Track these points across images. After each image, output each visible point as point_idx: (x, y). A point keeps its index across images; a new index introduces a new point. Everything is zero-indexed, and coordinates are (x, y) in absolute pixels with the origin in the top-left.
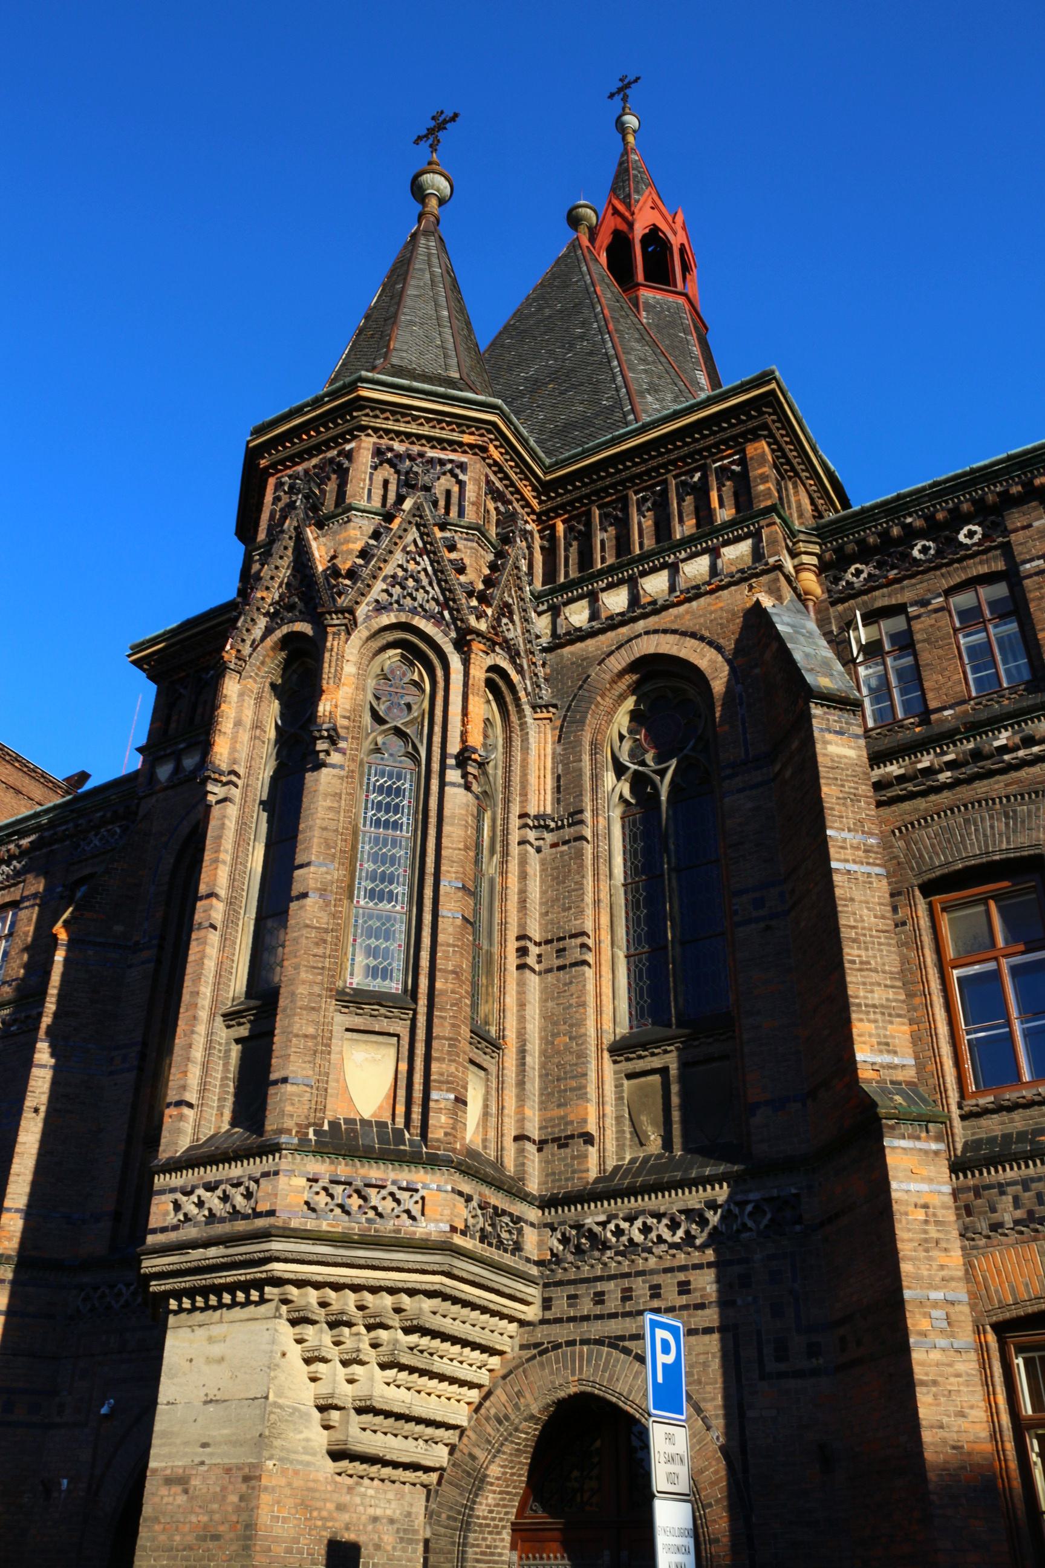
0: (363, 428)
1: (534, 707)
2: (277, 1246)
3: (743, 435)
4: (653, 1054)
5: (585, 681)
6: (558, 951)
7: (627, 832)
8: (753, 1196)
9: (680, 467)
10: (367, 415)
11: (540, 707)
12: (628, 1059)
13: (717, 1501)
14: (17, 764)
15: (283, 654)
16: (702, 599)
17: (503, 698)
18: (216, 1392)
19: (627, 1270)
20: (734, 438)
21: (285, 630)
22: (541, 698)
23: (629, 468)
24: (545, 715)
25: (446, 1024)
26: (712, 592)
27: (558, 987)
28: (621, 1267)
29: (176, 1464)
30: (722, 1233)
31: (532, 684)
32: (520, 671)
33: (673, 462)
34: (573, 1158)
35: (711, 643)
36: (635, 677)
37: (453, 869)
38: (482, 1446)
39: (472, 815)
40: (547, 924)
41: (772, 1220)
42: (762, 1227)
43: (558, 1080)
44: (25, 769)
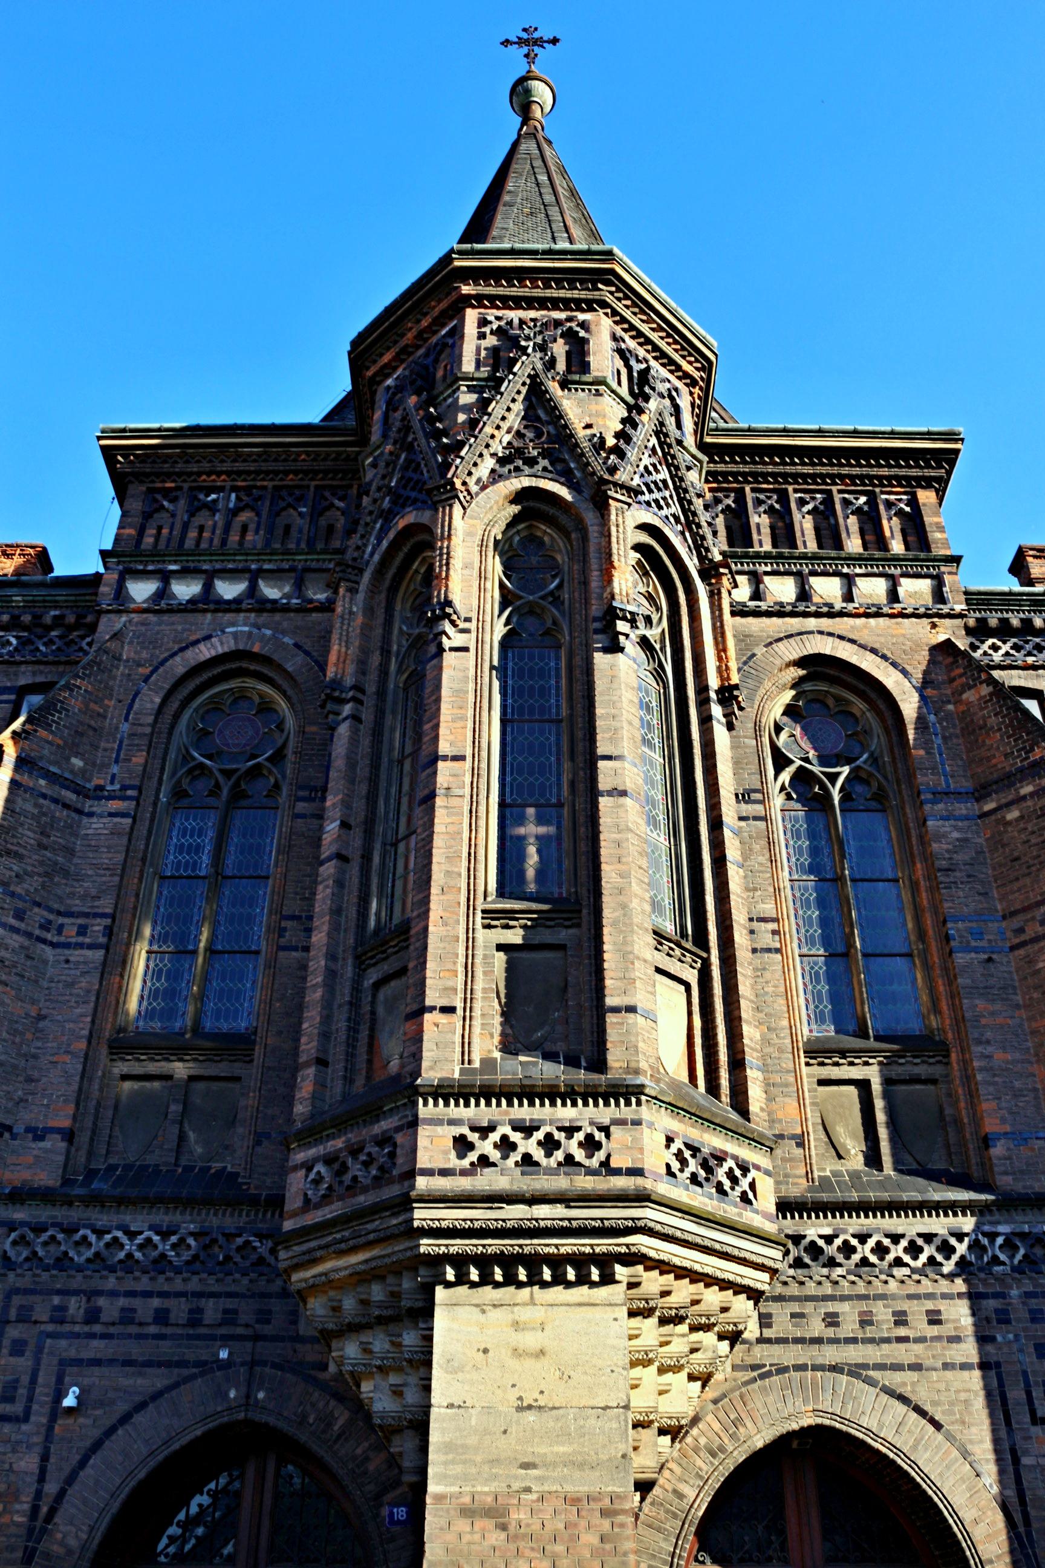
0: (604, 304)
2: (650, 1214)
3: (918, 479)
4: (851, 1064)
8: (1003, 1229)
9: (847, 485)
10: (611, 293)
12: (822, 1064)
13: (998, 1557)
15: (516, 509)
16: (881, 620)
18: (537, 1395)
19: (863, 1292)
20: (908, 478)
21: (526, 482)
23: (796, 464)
26: (892, 616)
28: (855, 1287)
29: (479, 1489)
30: (970, 1263)
33: (842, 477)
35: (894, 665)
36: (801, 672)
38: (691, 1482)
41: (1024, 1256)
42: (1016, 1261)
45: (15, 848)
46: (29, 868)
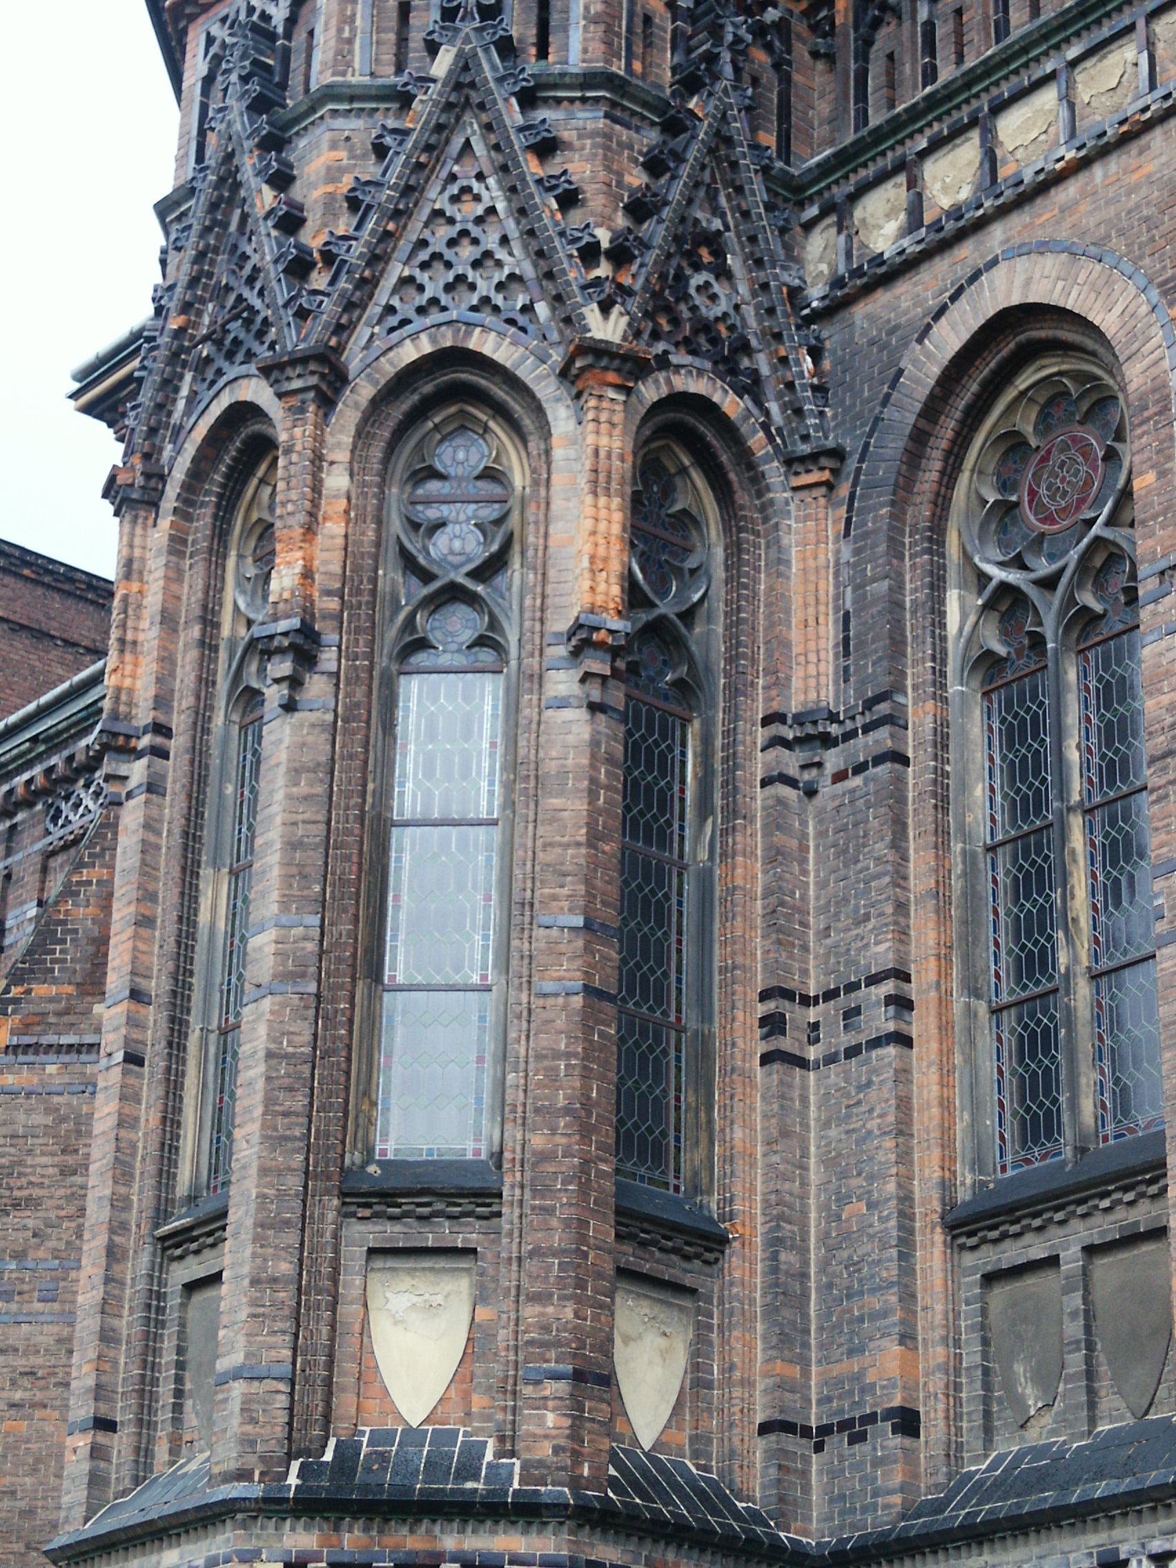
1: (792, 462)
5: (894, 384)
6: (847, 1015)
7: (996, 725)
11: (802, 459)
14: (26, 572)
17: (714, 457)
22: (805, 438)
24: (815, 477)
25: (554, 1223)
27: (848, 1096)
31: (784, 408)
32: (752, 387)
34: (877, 1463)
37: (565, 891)
39: (610, 760)
40: (827, 955)
43: (849, 1297)
44: (47, 579)
45: (25, 1193)
46: (52, 1215)
